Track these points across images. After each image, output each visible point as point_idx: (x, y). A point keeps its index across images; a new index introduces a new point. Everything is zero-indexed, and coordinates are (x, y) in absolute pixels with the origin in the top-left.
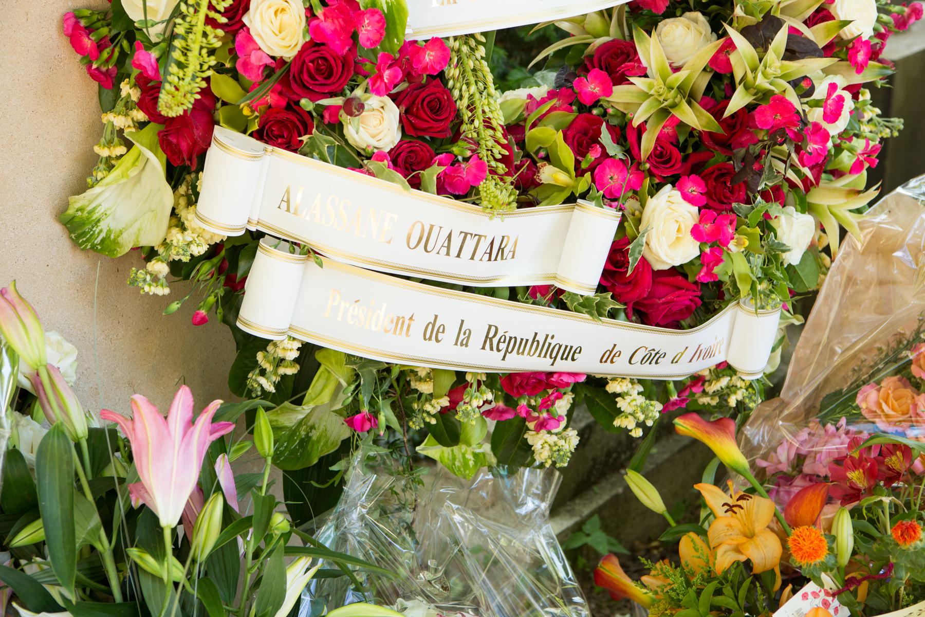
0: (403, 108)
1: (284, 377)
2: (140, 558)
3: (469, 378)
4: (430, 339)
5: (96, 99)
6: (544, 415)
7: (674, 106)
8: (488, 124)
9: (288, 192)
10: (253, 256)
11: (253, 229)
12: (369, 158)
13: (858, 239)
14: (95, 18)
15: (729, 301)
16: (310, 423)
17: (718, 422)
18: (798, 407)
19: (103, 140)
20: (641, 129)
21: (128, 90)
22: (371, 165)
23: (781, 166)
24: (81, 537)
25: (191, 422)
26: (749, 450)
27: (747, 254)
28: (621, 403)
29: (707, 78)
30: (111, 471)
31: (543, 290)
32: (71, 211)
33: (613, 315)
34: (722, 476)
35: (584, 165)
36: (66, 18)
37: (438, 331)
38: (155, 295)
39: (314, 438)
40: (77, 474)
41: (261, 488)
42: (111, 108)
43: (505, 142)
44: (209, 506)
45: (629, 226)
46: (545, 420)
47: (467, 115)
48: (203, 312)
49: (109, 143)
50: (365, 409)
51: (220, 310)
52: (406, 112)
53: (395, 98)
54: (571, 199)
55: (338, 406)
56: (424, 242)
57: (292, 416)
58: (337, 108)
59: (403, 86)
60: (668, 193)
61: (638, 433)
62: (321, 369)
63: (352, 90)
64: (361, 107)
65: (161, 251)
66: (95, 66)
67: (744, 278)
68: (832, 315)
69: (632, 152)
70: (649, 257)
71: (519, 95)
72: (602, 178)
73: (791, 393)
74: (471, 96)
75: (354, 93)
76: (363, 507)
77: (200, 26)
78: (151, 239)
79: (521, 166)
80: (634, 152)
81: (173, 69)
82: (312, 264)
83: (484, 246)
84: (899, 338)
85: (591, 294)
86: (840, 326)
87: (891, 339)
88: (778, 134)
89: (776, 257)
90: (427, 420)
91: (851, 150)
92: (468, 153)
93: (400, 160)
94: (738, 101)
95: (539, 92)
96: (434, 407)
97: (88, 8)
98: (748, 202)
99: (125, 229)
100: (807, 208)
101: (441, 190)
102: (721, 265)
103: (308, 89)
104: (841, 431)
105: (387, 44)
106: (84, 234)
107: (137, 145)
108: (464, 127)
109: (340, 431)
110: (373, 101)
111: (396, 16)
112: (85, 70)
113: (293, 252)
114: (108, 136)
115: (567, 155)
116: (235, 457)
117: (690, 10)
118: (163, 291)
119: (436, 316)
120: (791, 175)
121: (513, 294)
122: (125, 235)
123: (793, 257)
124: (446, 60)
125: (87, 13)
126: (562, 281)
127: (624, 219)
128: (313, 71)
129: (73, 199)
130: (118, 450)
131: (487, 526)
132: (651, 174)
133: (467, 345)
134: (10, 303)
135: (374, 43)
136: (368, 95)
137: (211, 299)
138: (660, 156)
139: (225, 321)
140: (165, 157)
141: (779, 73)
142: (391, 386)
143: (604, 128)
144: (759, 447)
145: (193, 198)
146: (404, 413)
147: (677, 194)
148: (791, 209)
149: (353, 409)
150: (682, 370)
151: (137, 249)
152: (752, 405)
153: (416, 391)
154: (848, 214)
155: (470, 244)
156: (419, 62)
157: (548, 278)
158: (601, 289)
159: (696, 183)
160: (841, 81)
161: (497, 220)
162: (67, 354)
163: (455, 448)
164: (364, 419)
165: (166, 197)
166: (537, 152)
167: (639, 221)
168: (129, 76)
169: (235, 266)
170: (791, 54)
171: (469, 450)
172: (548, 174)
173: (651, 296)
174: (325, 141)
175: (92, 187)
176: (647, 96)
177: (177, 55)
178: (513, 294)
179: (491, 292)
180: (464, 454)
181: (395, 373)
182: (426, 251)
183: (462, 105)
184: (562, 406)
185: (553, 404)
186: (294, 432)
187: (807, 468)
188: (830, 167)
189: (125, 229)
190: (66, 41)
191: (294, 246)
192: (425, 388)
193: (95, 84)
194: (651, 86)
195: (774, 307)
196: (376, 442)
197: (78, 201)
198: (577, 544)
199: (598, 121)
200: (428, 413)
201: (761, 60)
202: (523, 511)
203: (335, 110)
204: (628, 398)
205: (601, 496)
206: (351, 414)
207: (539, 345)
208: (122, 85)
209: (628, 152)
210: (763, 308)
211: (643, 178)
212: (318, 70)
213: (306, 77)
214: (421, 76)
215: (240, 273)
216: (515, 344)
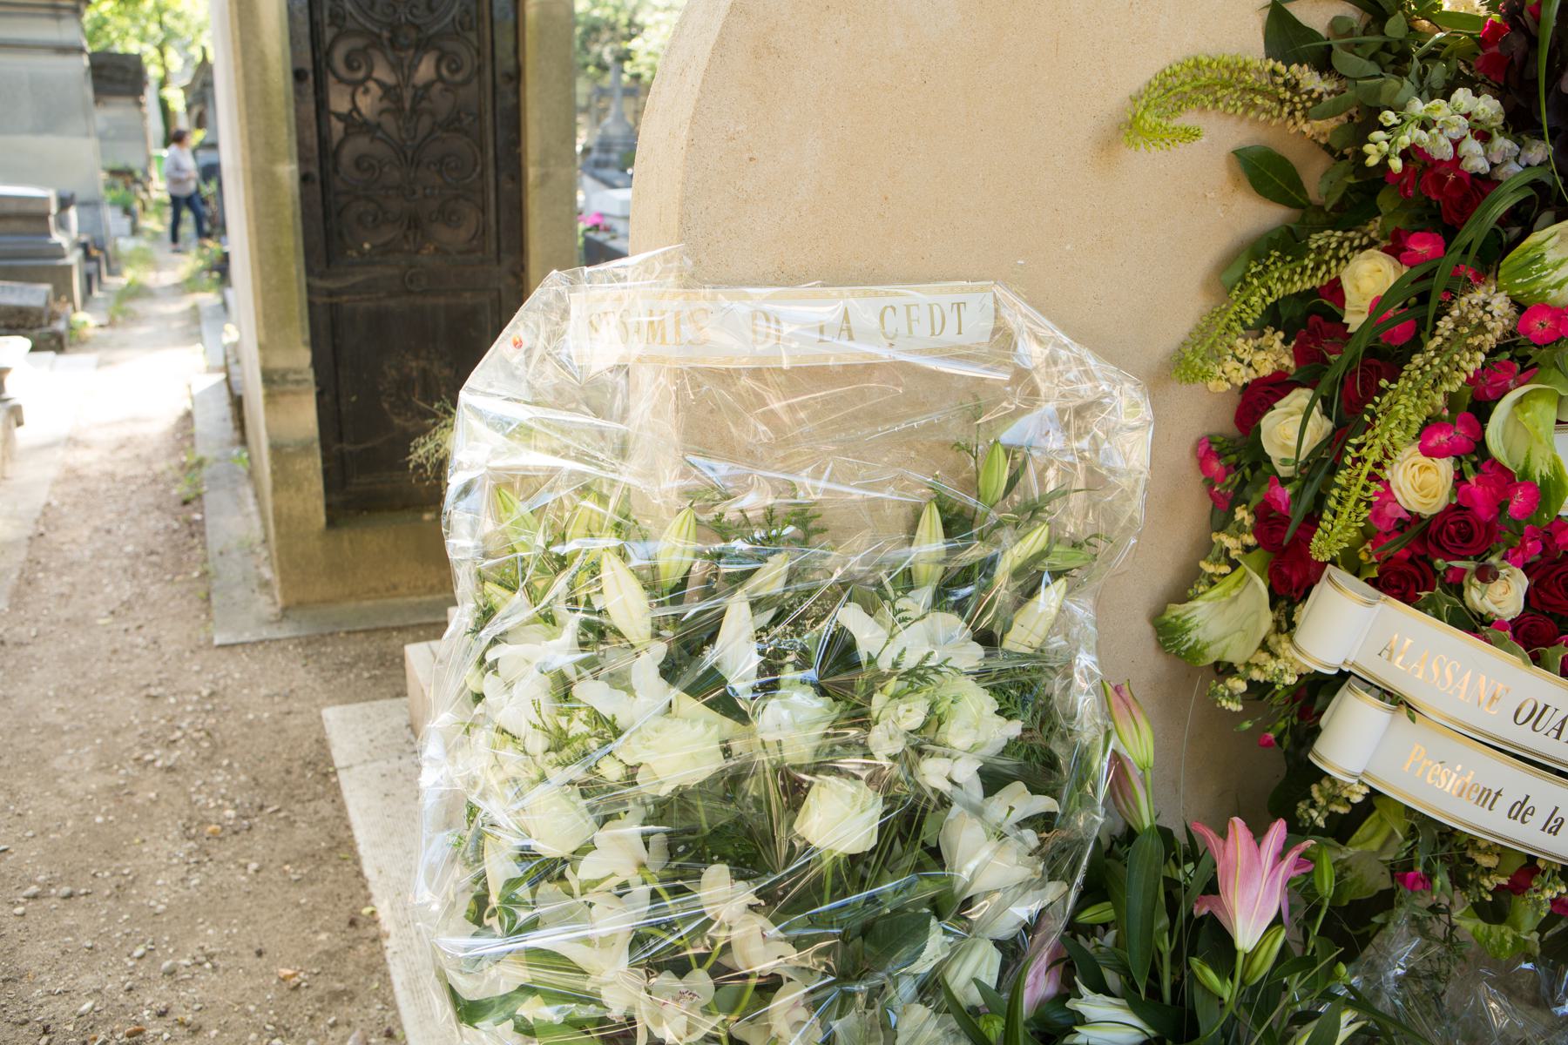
2: (1201, 969)
4: (1515, 818)
5: (1207, 517)
12: (1488, 625)
14: (1225, 445)
16: (1347, 864)
19: (1210, 557)
22: (1491, 632)
32: (1167, 617)
36: (1200, 442)
37: (1526, 812)
42: (1220, 530)
49: (1216, 561)
50: (1420, 869)
55: (1389, 857)
62: (1375, 815)
66: (1216, 489)
75: (840, 311)
77: (1363, 479)
78: (1236, 656)
90: (1484, 895)
97: (1221, 435)
103: (1444, 549)
106: (1173, 639)
111: (1552, 491)
113: (1383, 700)
118: (1236, 707)
119: (1528, 797)
122: (1212, 648)
125: (1220, 439)
128: (1453, 533)
129: (1171, 606)
131: (1499, 1004)
133: (1555, 833)
136: (1506, 563)
153: (1472, 860)
163: (1494, 928)
164: (1416, 878)
169: (1312, 699)
175: (1192, 599)
177: (1332, 503)
180: (1502, 935)
182: (1534, 729)
189: (1214, 642)
190: (1194, 463)
191: (1390, 697)
193: (1210, 503)
197: (1177, 610)
200: (1485, 888)
208: (1238, 510)
214: (1558, 551)
215: (1317, 708)
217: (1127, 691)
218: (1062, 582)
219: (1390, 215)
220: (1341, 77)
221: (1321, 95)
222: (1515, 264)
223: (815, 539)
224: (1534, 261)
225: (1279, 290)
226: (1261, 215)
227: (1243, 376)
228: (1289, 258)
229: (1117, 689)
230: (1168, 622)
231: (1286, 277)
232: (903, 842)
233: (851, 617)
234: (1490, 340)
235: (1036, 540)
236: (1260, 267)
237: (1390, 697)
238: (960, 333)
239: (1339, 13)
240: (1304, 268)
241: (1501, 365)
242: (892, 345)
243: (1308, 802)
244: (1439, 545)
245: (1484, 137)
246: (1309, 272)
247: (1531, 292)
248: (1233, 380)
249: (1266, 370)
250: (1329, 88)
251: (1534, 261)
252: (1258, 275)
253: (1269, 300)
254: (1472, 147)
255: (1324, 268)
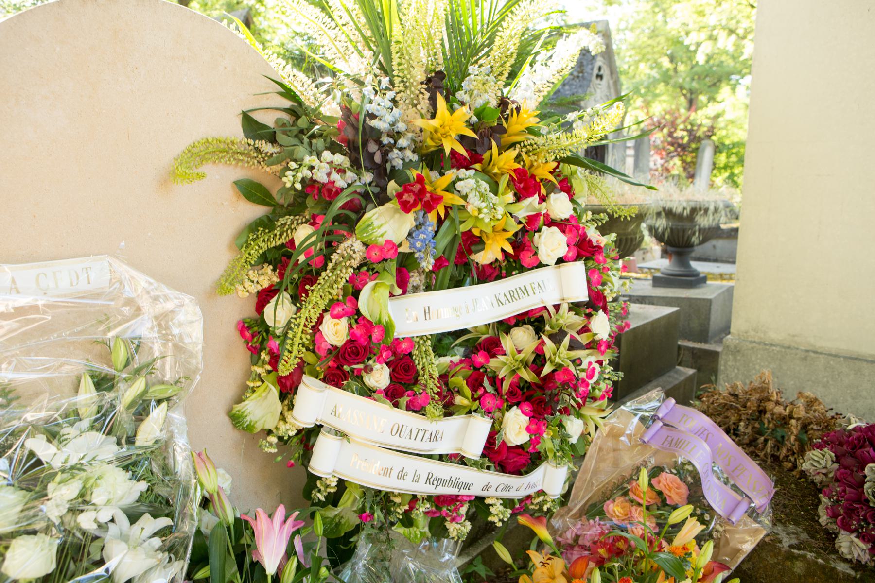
0: (392, 369)
1: (329, 493)
3: (418, 497)
5: (249, 359)
6: (455, 514)
7: (518, 369)
8: (431, 376)
9: (336, 407)
10: (318, 435)
11: (318, 424)
12: (374, 392)
13: (604, 430)
14: (252, 323)
15: (544, 461)
16: (341, 515)
17: (538, 518)
18: (577, 512)
20: (503, 379)
21: (264, 356)
23: (567, 398)
24: (228, 577)
25: (285, 521)
26: (553, 531)
27: (552, 439)
28: (492, 509)
29: (533, 356)
30: (245, 540)
31: (455, 456)
32: (234, 412)
33: (488, 468)
34: (541, 545)
35: (476, 396)
36: (239, 323)
38: (270, 453)
39: (343, 523)
40: (228, 546)
41: (315, 551)
42: (256, 364)
43: (439, 385)
44: (290, 562)
45: (497, 425)
46: (455, 517)
47: (421, 372)
48: (292, 461)
49: (254, 380)
50: (368, 511)
51: (301, 460)
52: (393, 371)
53: (388, 364)
54: (469, 412)
55: (355, 509)
56: (399, 431)
57: (332, 512)
58: (361, 370)
59: (392, 358)
60: (515, 411)
61: (499, 524)
62: (347, 490)
63: (368, 360)
64: (372, 369)
65: (274, 431)
66: (250, 345)
67: (551, 450)
68: (593, 465)
69: (498, 390)
70: (506, 440)
71: (446, 360)
72: (483, 403)
73: (573, 504)
74: (424, 364)
76: (365, 560)
78: (270, 426)
79: (446, 397)
80: (499, 390)
81: (286, 353)
82: (345, 441)
83: (427, 435)
84: (623, 477)
85: (478, 459)
86: (596, 472)
87: (620, 478)
88: (565, 384)
89: (566, 440)
91: (600, 390)
92: (421, 391)
93: (389, 393)
94: (547, 369)
95: (456, 359)
96: (401, 510)
98: (552, 415)
99: (259, 420)
100: (579, 416)
101: (408, 408)
102: (540, 445)
104: (597, 524)
105: (385, 340)
106: (239, 422)
107: (266, 383)
108: (420, 378)
109: (355, 520)
110: (377, 366)
112: (245, 345)
114: (254, 377)
115: (468, 391)
116: (303, 535)
117: (526, 324)
118: (274, 450)
120: (572, 402)
121: (441, 458)
122: (258, 423)
123: (574, 440)
124: (412, 347)
125: (249, 320)
126: (464, 452)
127: (494, 423)
129: (235, 406)
130: (248, 529)
132: (507, 400)
134: (202, 460)
135: (379, 340)
137: (297, 455)
138: (511, 392)
139: (303, 464)
140: (279, 388)
141: (566, 356)
142: (381, 499)
143: (485, 378)
144: (558, 530)
145: (291, 407)
146: (387, 512)
147: (519, 411)
148: (572, 417)
149: (363, 510)
150: (522, 494)
151: (263, 430)
152: (554, 510)
153: (393, 501)
154: (599, 419)
155: (421, 434)
156: (400, 348)
157: (457, 450)
158: (483, 455)
159: (529, 406)
160: (593, 359)
161: (434, 423)
162: (226, 480)
163: (411, 529)
164: (367, 515)
165: (279, 406)
166: (454, 389)
167: (501, 423)
168: (265, 349)
169: (309, 439)
170: (571, 348)
171: (418, 530)
172: (459, 400)
173: (507, 458)
174: (355, 385)
175: (244, 401)
176: (505, 364)
178: (441, 458)
179: (430, 457)
181: (383, 494)
183: (419, 368)
184: (463, 510)
185: (459, 509)
186: (333, 519)
187: (580, 542)
188: (590, 396)
189: (259, 420)
190: (238, 333)
191: (340, 434)
192: (398, 500)
193: (250, 353)
194: (507, 360)
195: (565, 464)
196: (372, 526)
197: (238, 407)
198: (470, 571)
199: (482, 375)
200: (398, 513)
201: (558, 349)
202: (443, 560)
203: (359, 370)
204: (495, 507)
205: (482, 547)
206: (361, 512)
207: (451, 482)
208: (262, 353)
209: (496, 390)
210: (559, 464)
211: (504, 402)
212: (352, 352)
213: (346, 355)
214: (400, 354)
215: (311, 443)
216: (441, 482)
217: (205, 456)
218: (164, 405)
219: (312, 207)
220: (280, 146)
221: (272, 154)
222: (362, 227)
223: (14, 404)
224: (369, 226)
225: (265, 247)
226: (257, 211)
227: (254, 289)
228: (267, 231)
229: (199, 455)
230: (235, 414)
231: (266, 240)
232: (75, 562)
233: (40, 446)
234: (355, 264)
235: (139, 385)
236: (255, 236)
237: (340, 434)
238: (89, 283)
239: (279, 117)
240: (275, 235)
241: (364, 274)
242: (45, 294)
243: (317, 490)
244: (345, 359)
245: (341, 171)
246: (278, 237)
247: (371, 240)
248: (250, 291)
249: (266, 285)
250: (276, 151)
251: (369, 226)
252: (254, 240)
253: (261, 252)
254: (335, 176)
255: (285, 234)
